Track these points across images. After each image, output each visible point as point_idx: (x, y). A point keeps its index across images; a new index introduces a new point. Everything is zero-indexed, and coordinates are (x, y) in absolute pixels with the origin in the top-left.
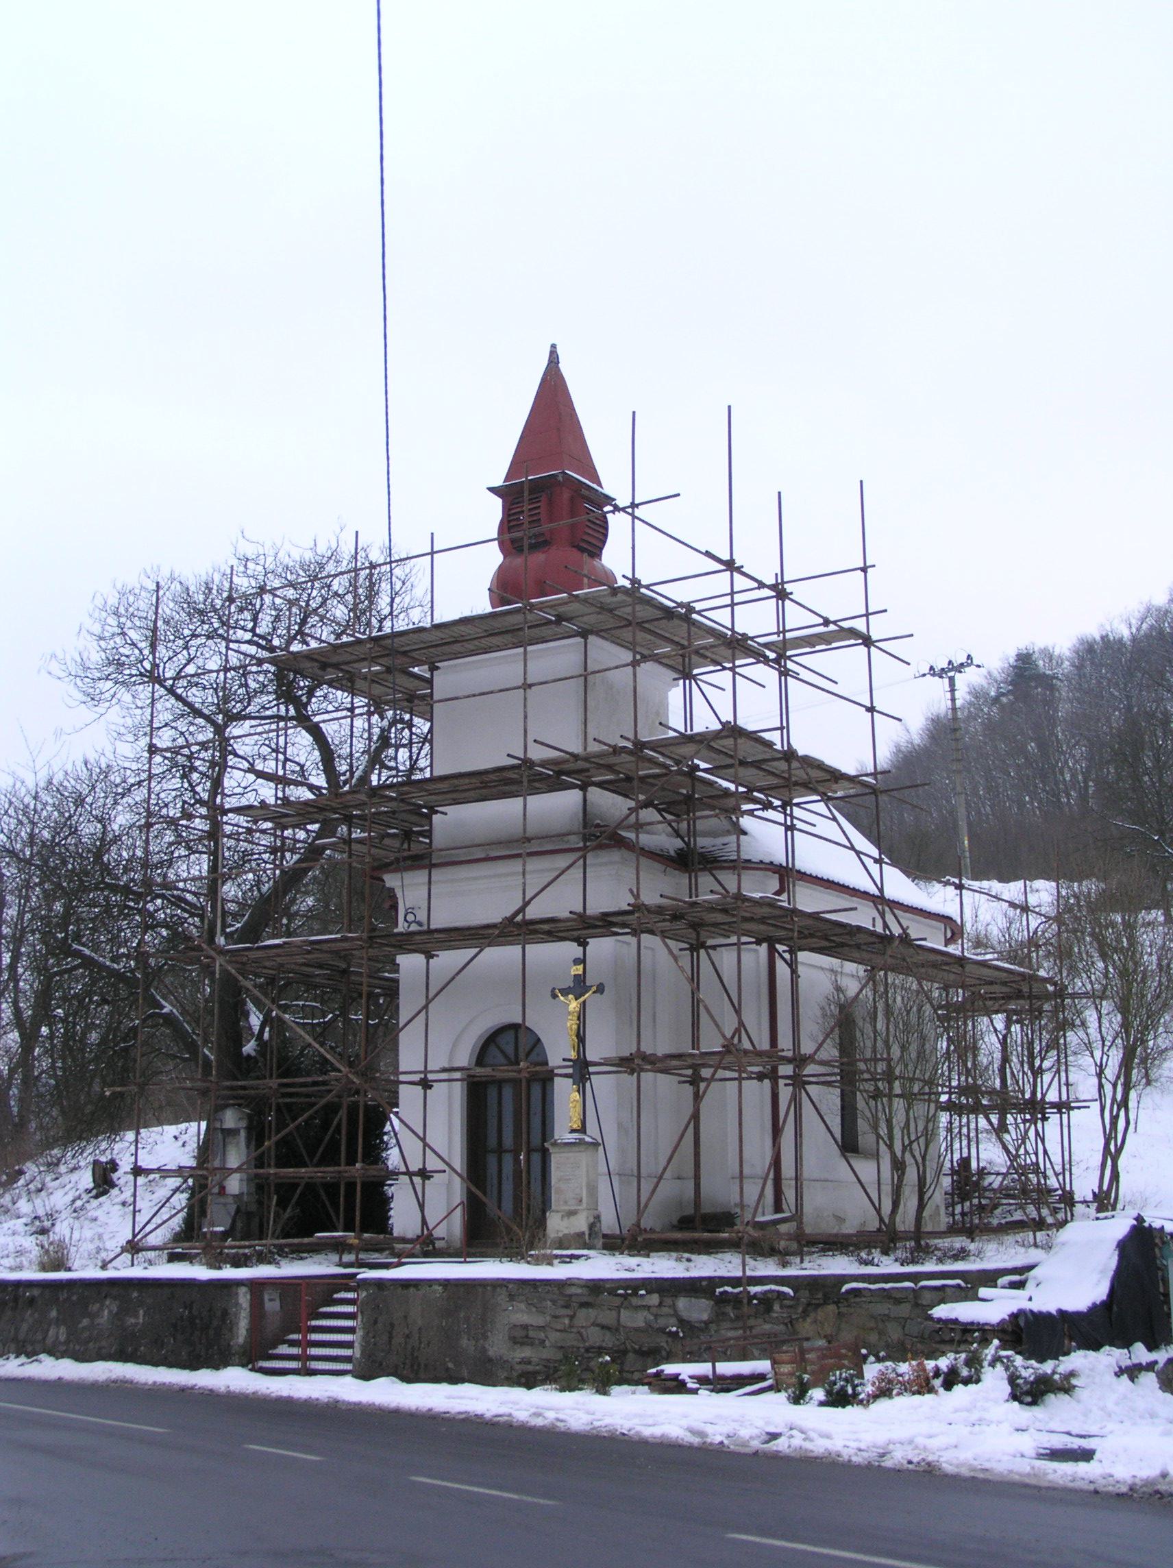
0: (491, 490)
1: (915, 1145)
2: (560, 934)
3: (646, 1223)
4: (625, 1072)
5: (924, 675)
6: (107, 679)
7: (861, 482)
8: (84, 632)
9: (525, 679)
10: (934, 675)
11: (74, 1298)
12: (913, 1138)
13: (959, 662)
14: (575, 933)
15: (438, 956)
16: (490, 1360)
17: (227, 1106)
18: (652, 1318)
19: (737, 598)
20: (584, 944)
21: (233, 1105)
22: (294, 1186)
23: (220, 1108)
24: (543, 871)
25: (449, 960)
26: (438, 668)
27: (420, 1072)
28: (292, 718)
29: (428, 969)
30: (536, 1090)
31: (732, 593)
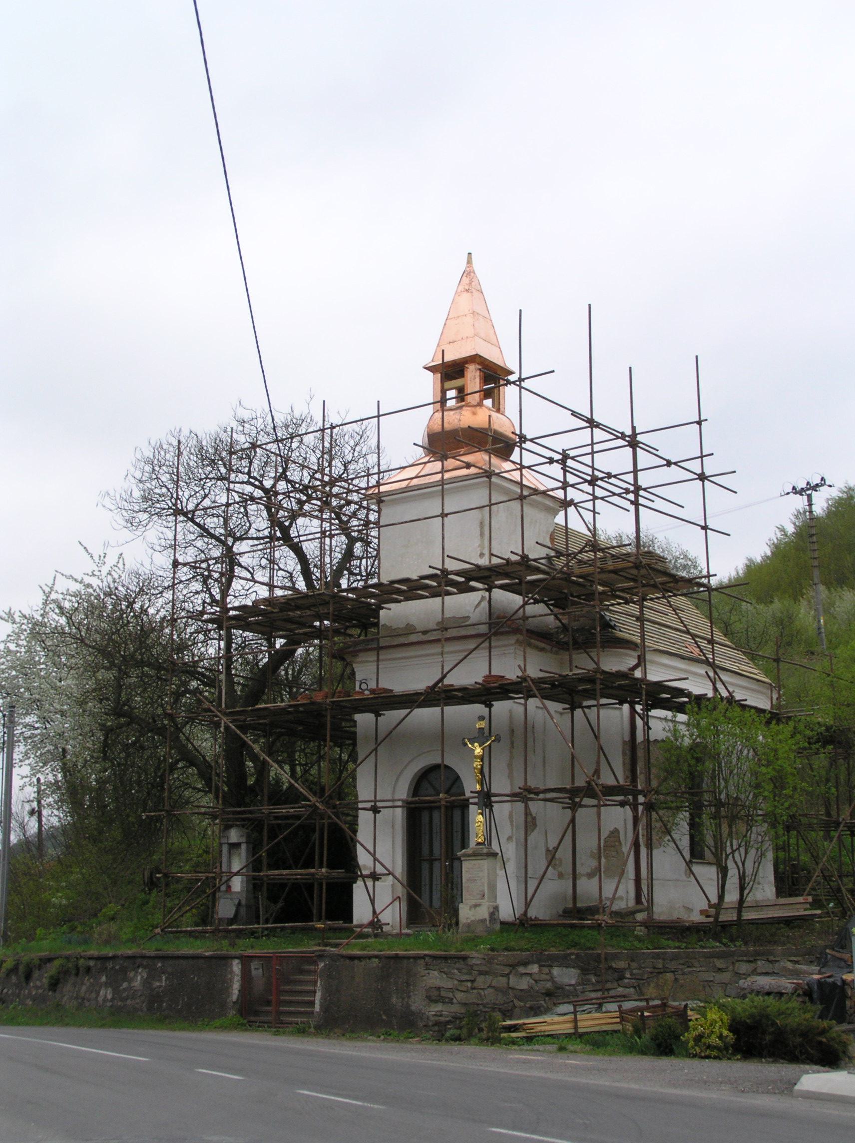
1: (736, 854)
2: (471, 699)
3: (532, 913)
4: (520, 801)
5: (788, 493)
6: (145, 511)
7: (697, 357)
8: (130, 477)
9: (443, 510)
10: (796, 493)
11: (117, 967)
12: (735, 848)
13: (815, 483)
14: (483, 698)
15: (384, 715)
16: (413, 1013)
17: (231, 827)
18: (533, 982)
19: (597, 448)
20: (489, 706)
21: (237, 826)
22: (283, 886)
23: (227, 827)
24: (456, 652)
25: (392, 716)
26: (383, 501)
27: (371, 801)
28: (278, 539)
29: (377, 724)
30: (457, 814)
31: (592, 444)
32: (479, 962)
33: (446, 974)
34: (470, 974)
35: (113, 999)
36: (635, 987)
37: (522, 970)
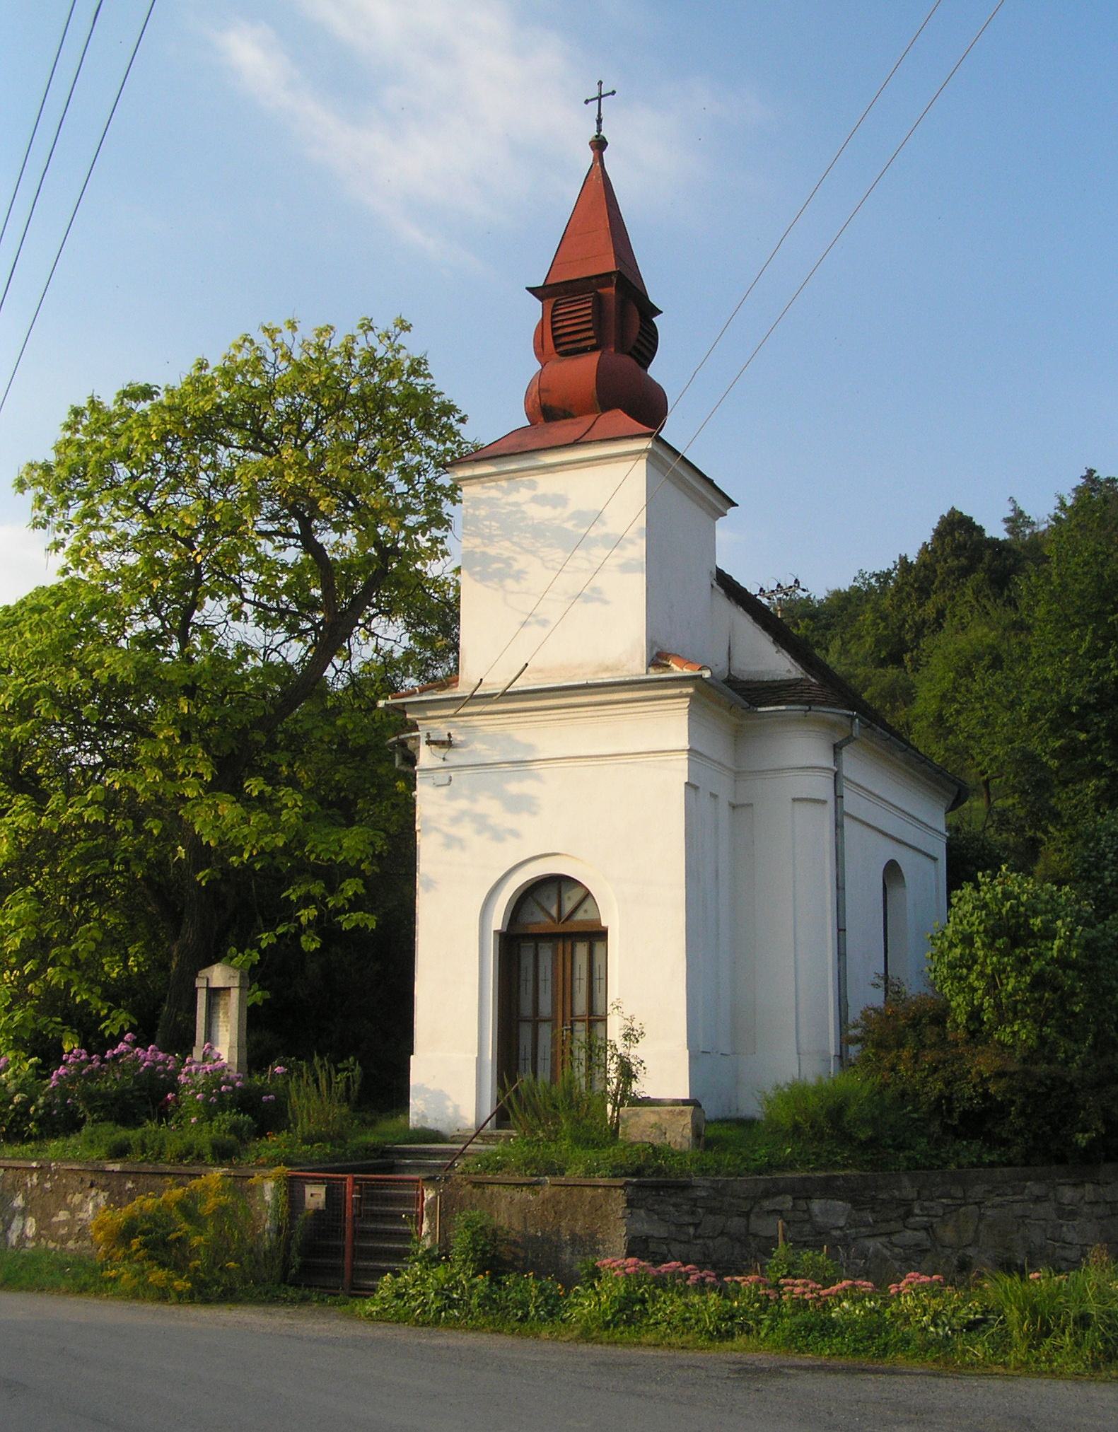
0: (530, 289)
11: (48, 1185)
32: (704, 1194)
33: (658, 1214)
34: (693, 1213)
35: (38, 1236)
36: (926, 1229)
37: (767, 1204)
